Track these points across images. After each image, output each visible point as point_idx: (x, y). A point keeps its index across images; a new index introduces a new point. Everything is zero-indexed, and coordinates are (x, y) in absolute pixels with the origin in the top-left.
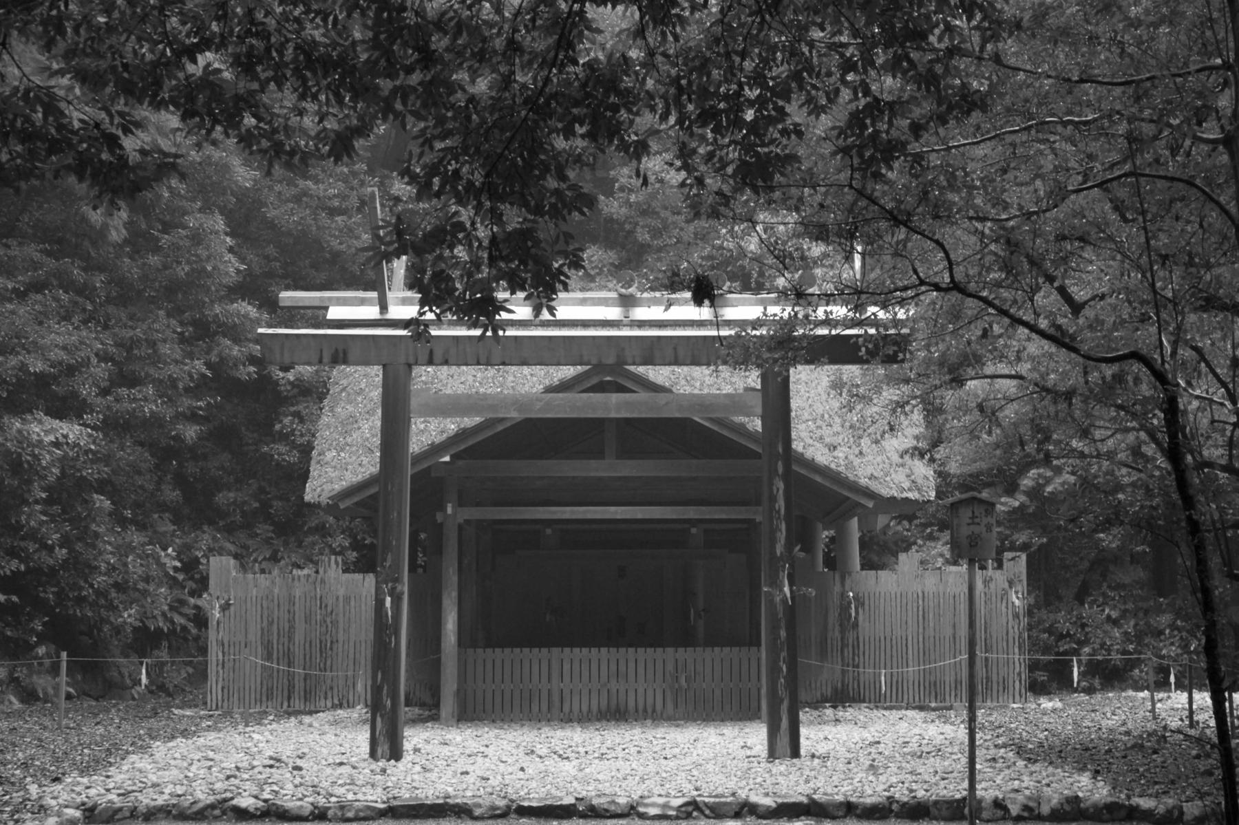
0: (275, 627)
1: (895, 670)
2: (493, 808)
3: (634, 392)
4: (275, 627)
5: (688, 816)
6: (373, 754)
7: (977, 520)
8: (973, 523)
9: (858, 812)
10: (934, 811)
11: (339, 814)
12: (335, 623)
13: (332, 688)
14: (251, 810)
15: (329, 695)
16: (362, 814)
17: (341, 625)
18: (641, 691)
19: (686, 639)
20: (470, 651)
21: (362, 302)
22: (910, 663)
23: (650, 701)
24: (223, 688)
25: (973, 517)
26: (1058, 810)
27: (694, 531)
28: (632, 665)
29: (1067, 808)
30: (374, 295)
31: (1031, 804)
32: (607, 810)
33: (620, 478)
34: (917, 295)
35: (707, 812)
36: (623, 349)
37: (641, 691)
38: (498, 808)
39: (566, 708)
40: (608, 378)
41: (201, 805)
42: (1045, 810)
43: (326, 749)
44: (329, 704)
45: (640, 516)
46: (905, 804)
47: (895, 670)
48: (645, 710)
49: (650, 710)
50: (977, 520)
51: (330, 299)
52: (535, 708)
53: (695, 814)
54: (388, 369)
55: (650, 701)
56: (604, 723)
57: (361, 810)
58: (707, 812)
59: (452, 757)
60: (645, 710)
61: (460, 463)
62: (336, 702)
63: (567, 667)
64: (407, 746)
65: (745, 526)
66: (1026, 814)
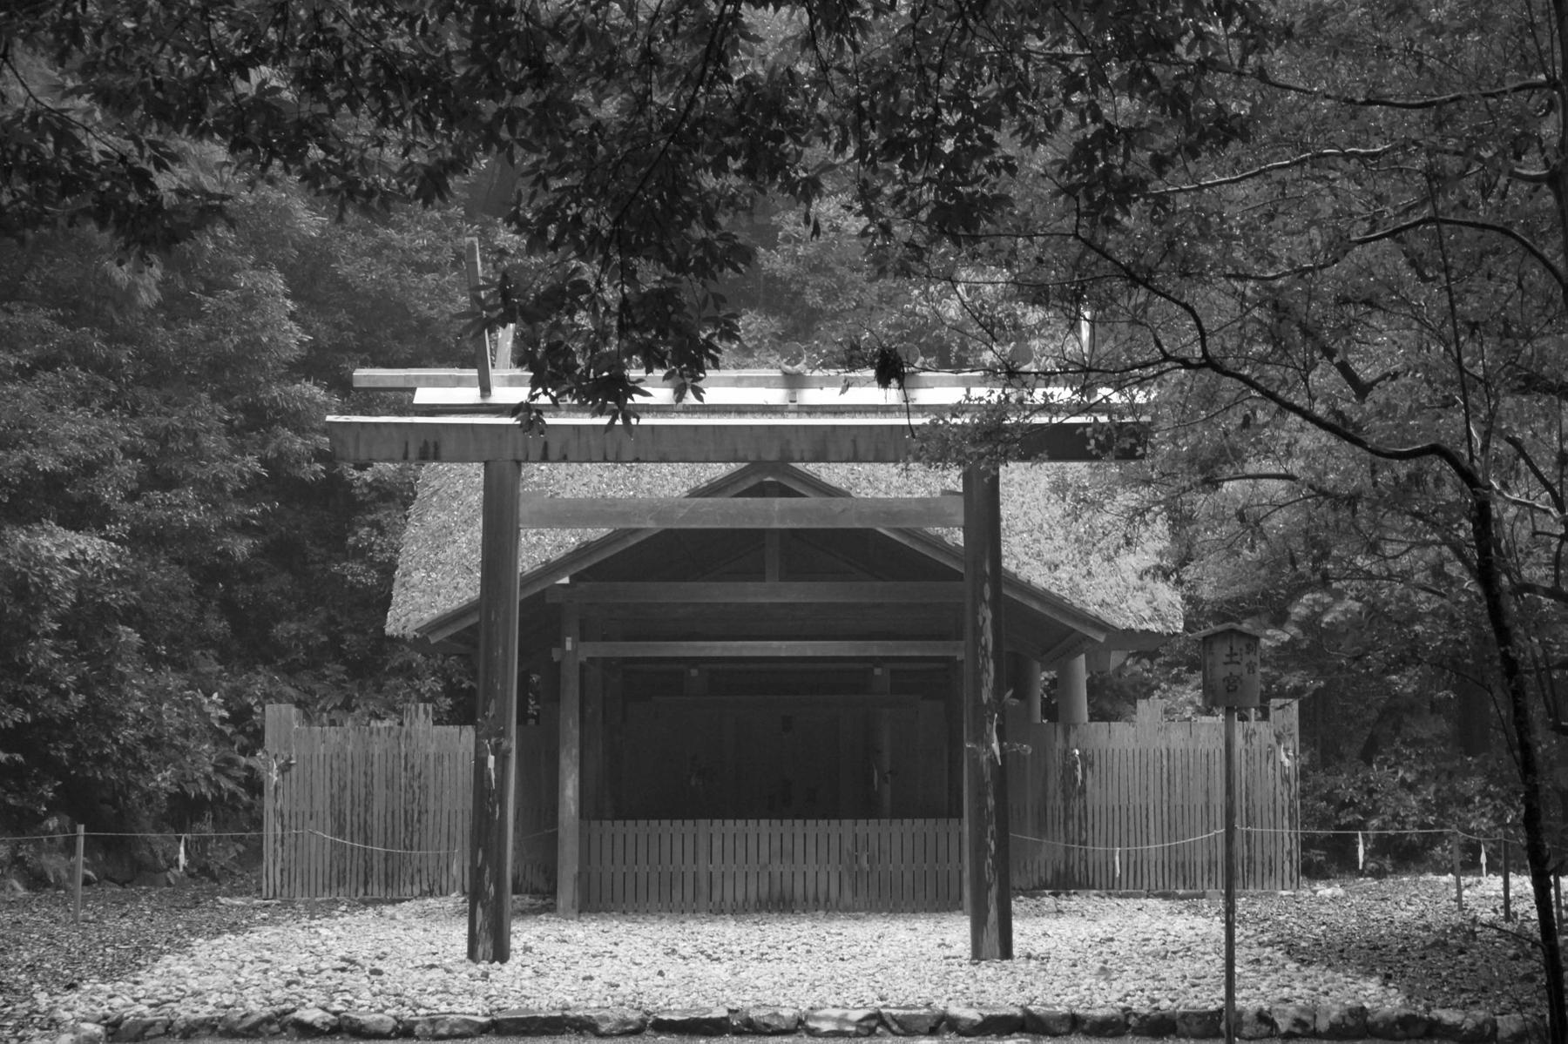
3: (695, 493)
4: (348, 792)
5: (871, 1032)
6: (472, 955)
7: (1236, 658)
8: (1231, 662)
9: (1086, 1027)
10: (1181, 1026)
11: (430, 1029)
12: (424, 788)
13: (420, 871)
14: (318, 1024)
15: (417, 879)
16: (458, 1030)
17: (432, 791)
19: (867, 808)
20: (595, 824)
21: (458, 382)
23: (822, 887)
25: (1232, 655)
26: (1338, 1025)
27: (878, 671)
29: (1350, 1022)
30: (474, 373)
31: (1305, 1017)
32: (767, 1026)
35: (895, 1027)
38: (630, 1023)
40: (769, 479)
41: (254, 1019)
42: (1323, 1024)
43: (413, 948)
44: (417, 891)
45: (809, 653)
48: (816, 899)
49: (822, 899)
50: (1236, 658)
51: (417, 378)
52: (677, 896)
53: (879, 1030)
55: (822, 887)
57: (456, 1025)
58: (895, 1027)
59: (572, 958)
60: (827, 899)
61: (582, 586)
62: (425, 888)
63: (717, 844)
64: (516, 944)
65: (943, 665)
66: (1298, 1030)
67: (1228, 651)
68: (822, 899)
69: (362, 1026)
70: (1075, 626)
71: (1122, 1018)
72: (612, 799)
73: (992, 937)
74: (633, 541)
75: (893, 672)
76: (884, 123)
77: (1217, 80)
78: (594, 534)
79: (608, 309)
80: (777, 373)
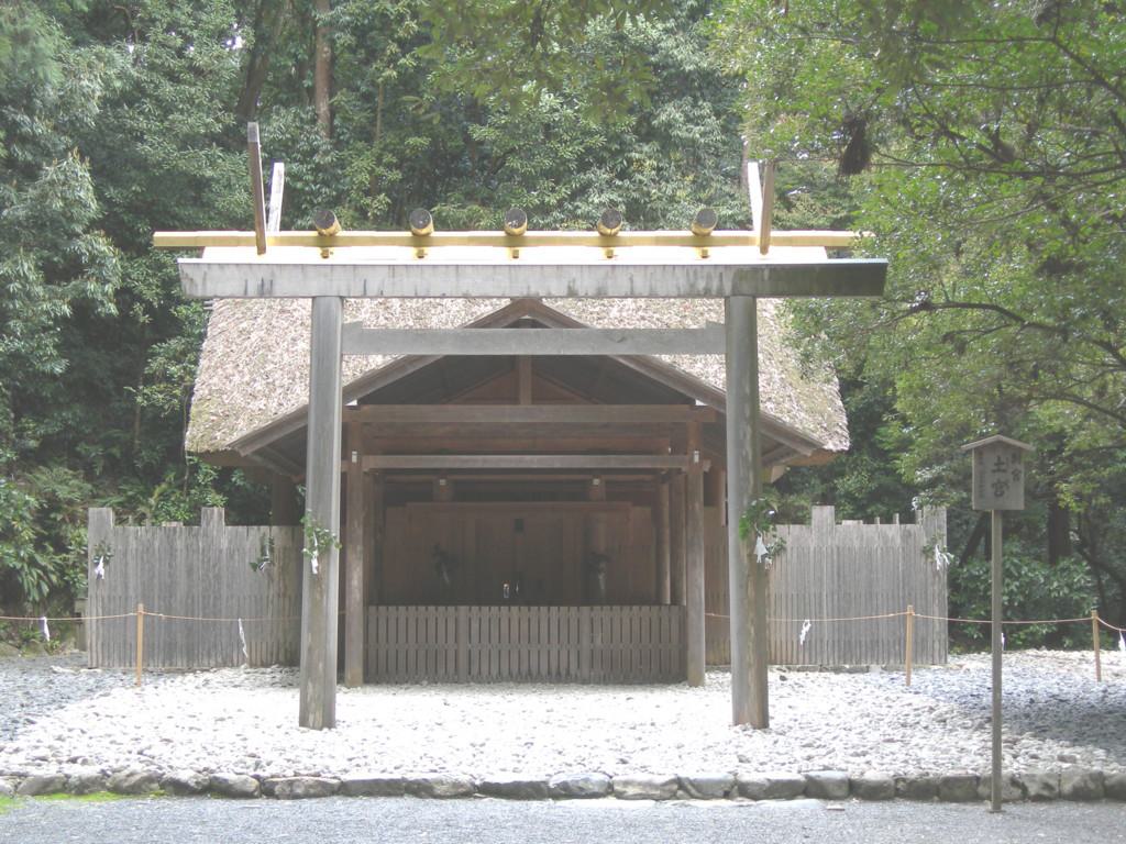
0: (156, 581)
1: (789, 620)
2: (457, 785)
3: (547, 327)
4: (156, 581)
5: (674, 796)
6: (303, 722)
7: (1003, 467)
8: (999, 470)
9: (861, 791)
10: (945, 791)
11: (288, 790)
12: (218, 577)
13: (215, 646)
14: (192, 783)
15: (213, 653)
16: (312, 791)
17: (224, 580)
18: (554, 654)
19: (588, 598)
20: (372, 609)
21: (238, 242)
22: (825, 615)
23: (563, 665)
24: (103, 645)
25: (999, 463)
26: (1082, 789)
27: (596, 482)
28: (544, 625)
29: (1092, 786)
30: (252, 234)
31: (1053, 782)
32: (581, 789)
33: (530, 425)
34: (1117, 178)
35: (693, 791)
36: (574, 281)
37: (554, 654)
38: (462, 786)
39: (475, 671)
40: (527, 317)
41: (137, 777)
42: (1067, 788)
43: (229, 717)
44: (213, 663)
45: (557, 465)
46: (913, 782)
47: (789, 620)
48: (559, 673)
49: (563, 672)
50: (1003, 467)
51: (206, 238)
52: (441, 671)
53: (680, 792)
54: (287, 315)
55: (563, 665)
56: (512, 684)
57: (311, 786)
58: (693, 791)
59: (393, 727)
60: (559, 673)
61: (366, 408)
62: (220, 660)
63: (475, 626)
64: (339, 714)
65: (648, 477)
66: (1046, 793)
67: (996, 461)
68: (563, 672)
69: (231, 786)
70: (782, 441)
71: (1082, 784)
72: (391, 585)
73: (751, 706)
74: (420, 365)
75: (607, 482)
76: (30, 68)
77: (374, 33)
78: (377, 361)
79: (1081, 157)
80: (690, 234)
